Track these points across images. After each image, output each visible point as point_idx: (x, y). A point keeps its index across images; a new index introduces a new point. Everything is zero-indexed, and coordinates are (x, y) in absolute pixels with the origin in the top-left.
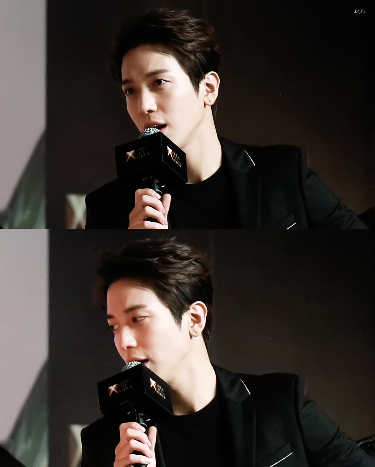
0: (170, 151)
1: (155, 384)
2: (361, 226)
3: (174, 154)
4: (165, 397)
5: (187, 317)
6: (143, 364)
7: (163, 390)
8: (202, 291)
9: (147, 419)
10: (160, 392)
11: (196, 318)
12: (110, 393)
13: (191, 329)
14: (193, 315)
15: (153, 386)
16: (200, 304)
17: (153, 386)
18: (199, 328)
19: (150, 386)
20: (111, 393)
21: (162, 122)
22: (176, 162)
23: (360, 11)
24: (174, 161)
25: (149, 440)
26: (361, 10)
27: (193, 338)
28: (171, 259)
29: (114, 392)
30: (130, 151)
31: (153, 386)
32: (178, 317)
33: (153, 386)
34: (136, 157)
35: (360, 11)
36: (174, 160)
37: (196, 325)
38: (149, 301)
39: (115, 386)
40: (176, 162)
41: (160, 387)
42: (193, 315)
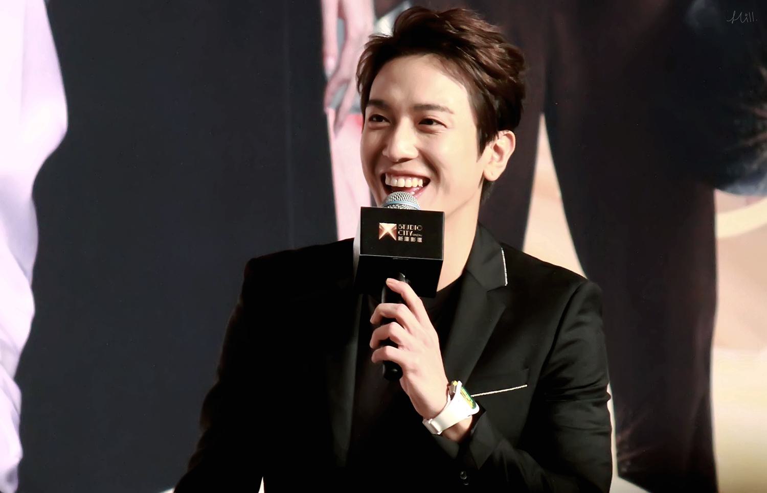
23: (743, 17)
24: (400, 241)
35: (743, 17)
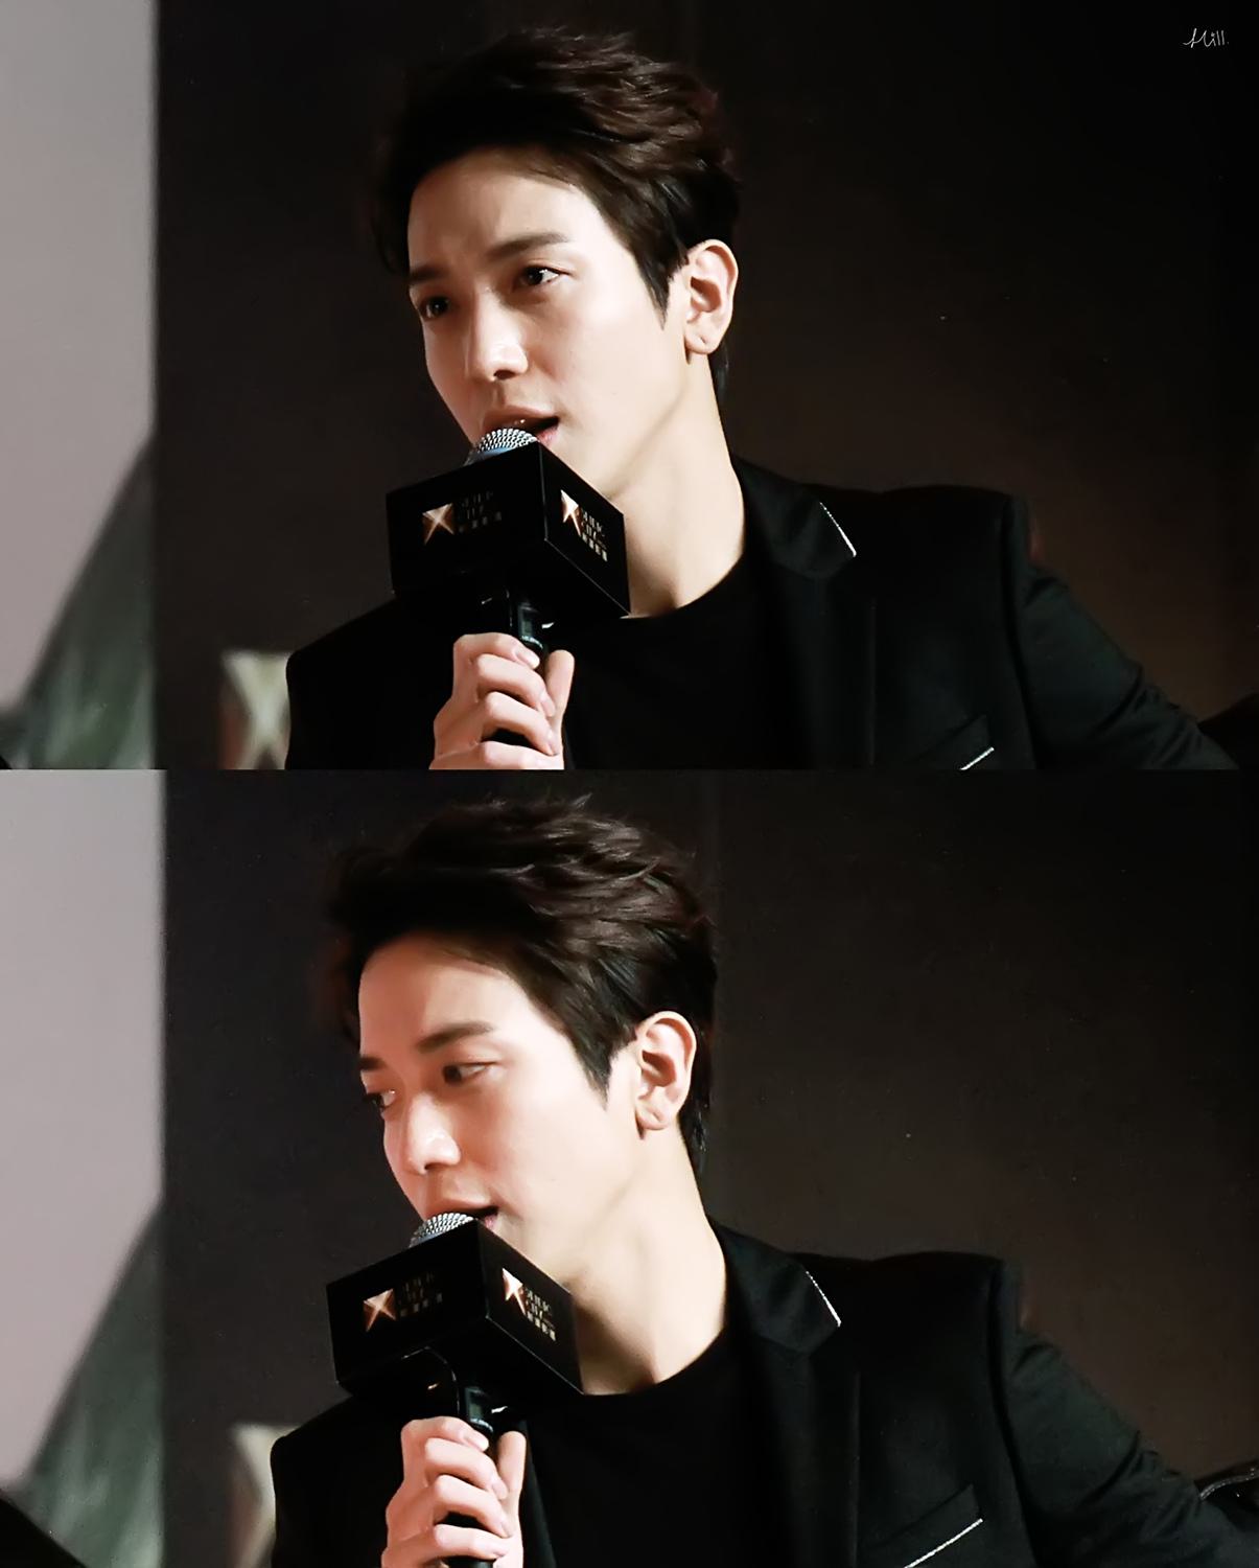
0: (571, 507)
1: (519, 1290)
2: (1211, 758)
3: (585, 516)
4: (553, 1334)
5: (626, 1065)
7: (546, 1308)
8: (677, 978)
9: (495, 1408)
10: (538, 1317)
11: (659, 1068)
12: (369, 1319)
13: (640, 1105)
14: (648, 1057)
15: (513, 1298)
16: (673, 1020)
17: (513, 1297)
18: (667, 1101)
19: (504, 1296)
20: (373, 1319)
21: (543, 408)
22: (591, 543)
23: (1209, 38)
24: (583, 541)
25: (499, 1478)
26: (1213, 35)
27: (649, 1134)
28: (574, 868)
29: (381, 1315)
30: (436, 506)
31: (513, 1297)
32: (597, 1063)
33: (513, 1298)
34: (455, 526)
35: (1209, 38)
36: (584, 538)
37: (660, 1091)
38: (499, 1011)
39: (385, 1295)
40: (591, 543)
41: (538, 1300)
42: (648, 1057)
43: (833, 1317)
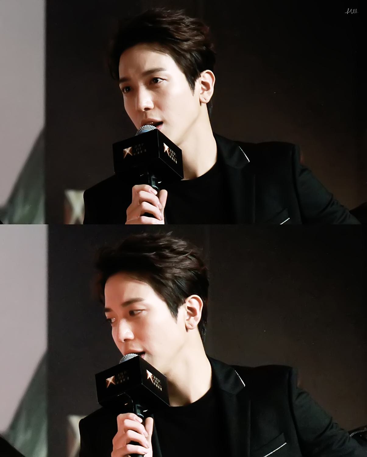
5: (183, 310)
6: (140, 356)
8: (197, 285)
9: (144, 410)
11: (192, 311)
12: (108, 384)
13: (187, 322)
14: (189, 308)
15: (150, 378)
16: (196, 297)
17: (150, 378)
18: (194, 321)
21: (158, 119)
23: (352, 11)
25: (146, 431)
26: (354, 10)
27: (189, 330)
28: (167, 253)
30: (127, 148)
31: (150, 378)
32: (174, 310)
33: (150, 378)
34: (133, 153)
35: (352, 11)
37: (192, 318)
38: (146, 295)
42: (189, 308)
43: (243, 384)
